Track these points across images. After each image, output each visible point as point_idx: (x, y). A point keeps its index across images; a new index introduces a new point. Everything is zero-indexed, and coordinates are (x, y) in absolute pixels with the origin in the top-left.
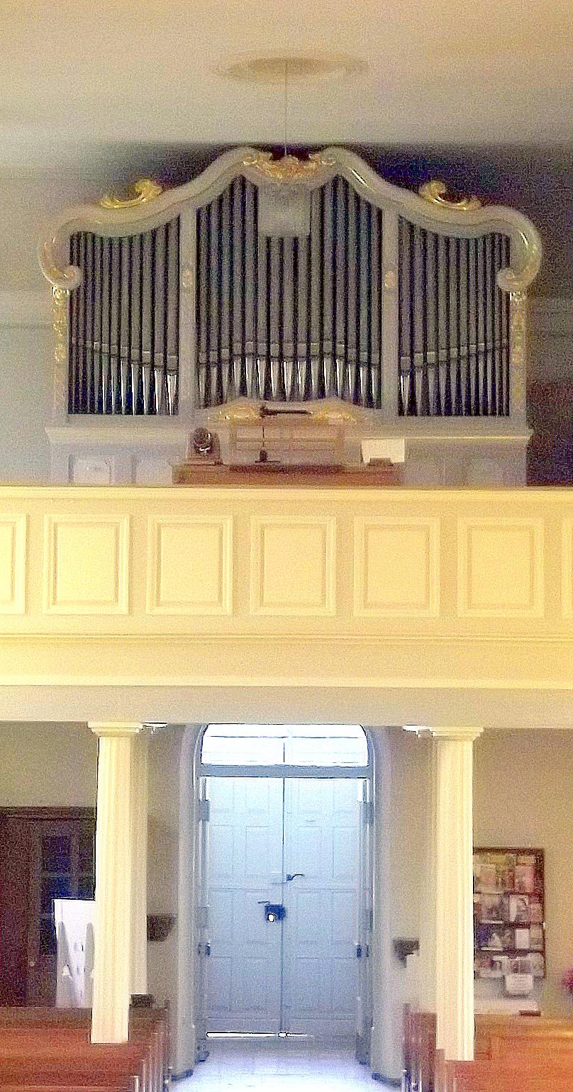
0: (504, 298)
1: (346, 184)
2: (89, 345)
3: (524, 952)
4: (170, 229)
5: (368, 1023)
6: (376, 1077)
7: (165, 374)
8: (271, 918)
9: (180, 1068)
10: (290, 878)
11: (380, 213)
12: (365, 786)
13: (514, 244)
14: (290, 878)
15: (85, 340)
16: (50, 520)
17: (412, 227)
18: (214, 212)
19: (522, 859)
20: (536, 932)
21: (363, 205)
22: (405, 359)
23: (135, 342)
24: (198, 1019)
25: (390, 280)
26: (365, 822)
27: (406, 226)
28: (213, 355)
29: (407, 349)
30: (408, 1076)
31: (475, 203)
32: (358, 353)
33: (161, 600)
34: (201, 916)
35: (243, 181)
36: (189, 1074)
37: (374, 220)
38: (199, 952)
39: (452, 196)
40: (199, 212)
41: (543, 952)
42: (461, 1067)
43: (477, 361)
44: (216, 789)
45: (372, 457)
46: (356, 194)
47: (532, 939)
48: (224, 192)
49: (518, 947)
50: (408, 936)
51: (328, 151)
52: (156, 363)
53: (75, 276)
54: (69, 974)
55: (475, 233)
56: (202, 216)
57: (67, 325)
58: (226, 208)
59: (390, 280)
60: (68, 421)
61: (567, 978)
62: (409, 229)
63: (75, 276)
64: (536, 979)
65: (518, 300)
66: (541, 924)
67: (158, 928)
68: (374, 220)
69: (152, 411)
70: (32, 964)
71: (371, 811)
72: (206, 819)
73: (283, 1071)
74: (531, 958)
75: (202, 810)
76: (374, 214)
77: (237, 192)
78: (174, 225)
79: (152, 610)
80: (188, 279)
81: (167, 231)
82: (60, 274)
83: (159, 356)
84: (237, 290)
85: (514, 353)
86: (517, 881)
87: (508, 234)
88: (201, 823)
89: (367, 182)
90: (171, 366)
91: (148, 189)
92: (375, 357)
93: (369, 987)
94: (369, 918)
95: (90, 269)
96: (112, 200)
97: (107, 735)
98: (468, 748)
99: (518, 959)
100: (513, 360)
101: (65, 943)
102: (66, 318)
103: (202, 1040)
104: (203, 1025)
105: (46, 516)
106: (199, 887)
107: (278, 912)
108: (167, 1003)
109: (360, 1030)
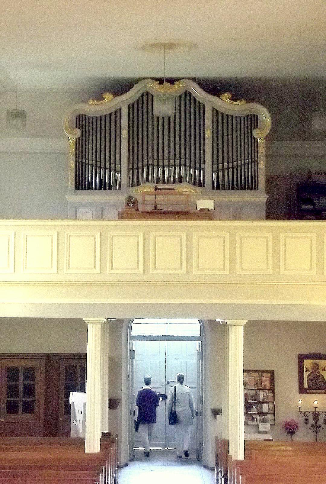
1: (190, 94)
2: (84, 161)
3: (266, 414)
6: (205, 467)
10: (168, 383)
11: (204, 106)
14: (168, 383)
17: (217, 111)
19: (265, 375)
20: (271, 405)
21: (197, 103)
30: (217, 466)
31: (243, 102)
35: (147, 93)
36: (126, 465)
39: (234, 98)
41: (274, 414)
42: (239, 462)
44: (137, 345)
46: (194, 98)
50: (217, 407)
51: (183, 80)
55: (245, 114)
56: (131, 107)
62: (216, 112)
63: (78, 133)
70: (61, 419)
71: (202, 355)
74: (269, 417)
75: (132, 354)
90: (118, 169)
91: (108, 96)
98: (241, 329)
99: (264, 417)
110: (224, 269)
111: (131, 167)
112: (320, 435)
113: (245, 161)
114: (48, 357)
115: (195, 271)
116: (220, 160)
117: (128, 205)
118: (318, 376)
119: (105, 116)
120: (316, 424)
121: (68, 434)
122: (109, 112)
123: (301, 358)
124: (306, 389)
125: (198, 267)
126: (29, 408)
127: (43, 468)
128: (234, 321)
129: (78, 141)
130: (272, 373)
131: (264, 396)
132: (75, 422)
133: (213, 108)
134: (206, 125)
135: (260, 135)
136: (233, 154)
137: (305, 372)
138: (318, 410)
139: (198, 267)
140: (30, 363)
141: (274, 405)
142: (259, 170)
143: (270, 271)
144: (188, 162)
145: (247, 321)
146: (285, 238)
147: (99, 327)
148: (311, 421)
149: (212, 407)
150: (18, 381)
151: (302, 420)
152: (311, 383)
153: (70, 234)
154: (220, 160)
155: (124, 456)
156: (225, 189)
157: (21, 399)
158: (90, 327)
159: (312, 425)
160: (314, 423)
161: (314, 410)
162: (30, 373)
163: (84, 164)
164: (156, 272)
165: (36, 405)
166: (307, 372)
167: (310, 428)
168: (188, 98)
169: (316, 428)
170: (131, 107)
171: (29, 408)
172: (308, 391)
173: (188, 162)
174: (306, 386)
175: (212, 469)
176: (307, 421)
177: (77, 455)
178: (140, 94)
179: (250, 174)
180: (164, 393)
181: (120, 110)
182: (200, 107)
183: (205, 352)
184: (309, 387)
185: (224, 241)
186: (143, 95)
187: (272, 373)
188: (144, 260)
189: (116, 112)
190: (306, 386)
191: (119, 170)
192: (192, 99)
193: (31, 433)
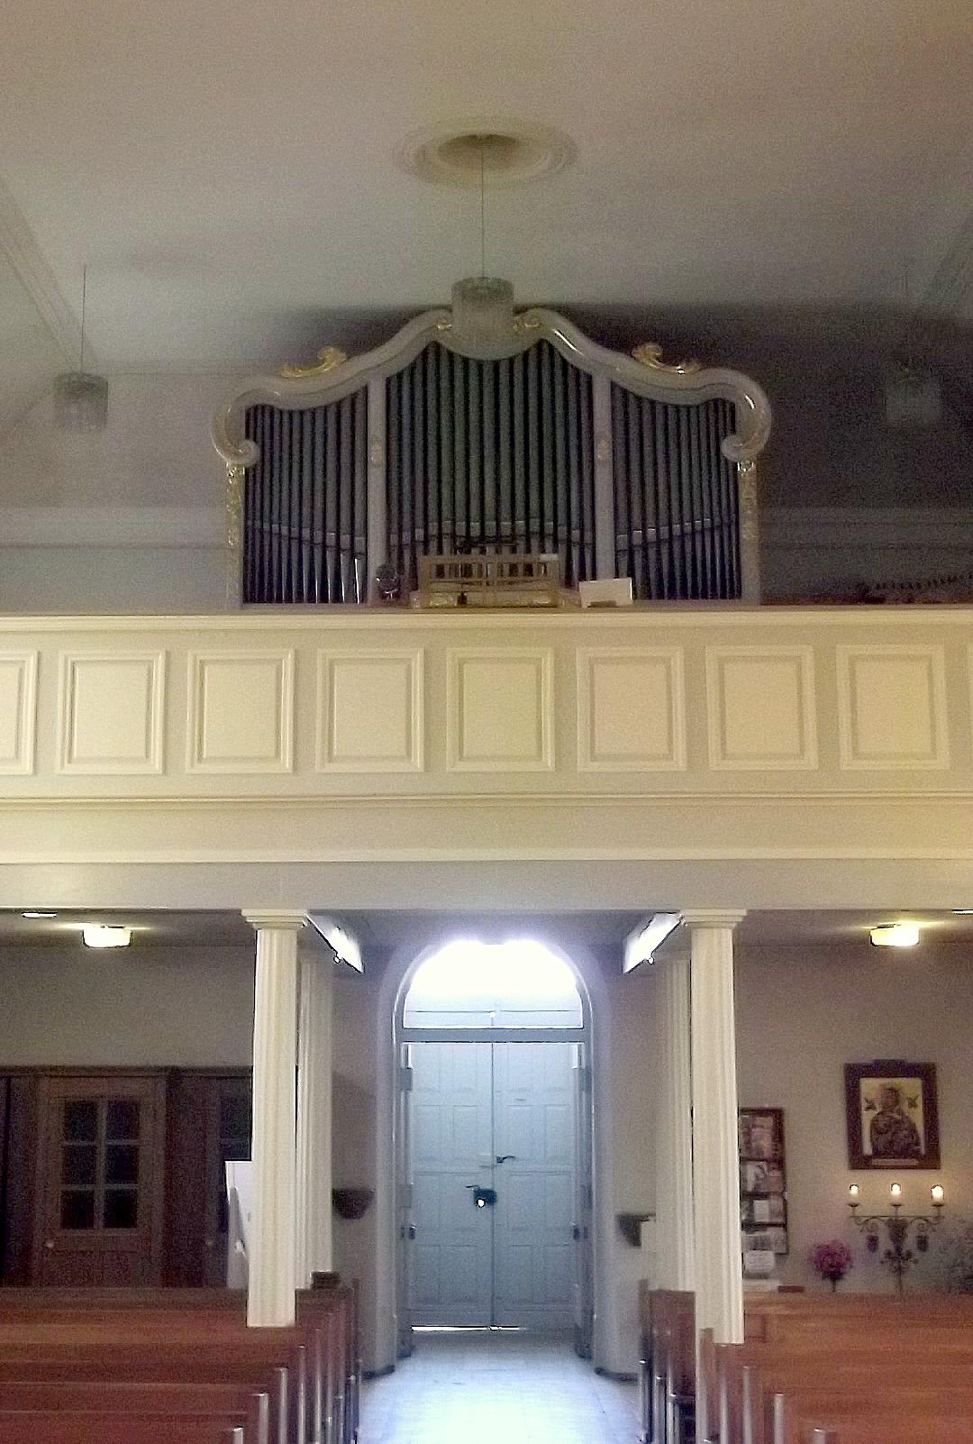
0: (731, 467)
1: (551, 348)
2: (266, 527)
3: (763, 1226)
4: (358, 400)
5: (589, 1313)
6: (600, 1372)
7: (353, 557)
8: (481, 1203)
9: (380, 1365)
10: (500, 1160)
11: (590, 378)
12: (580, 1052)
13: (739, 406)
14: (500, 1160)
15: (262, 521)
16: (195, 656)
17: (625, 393)
18: (406, 380)
19: (759, 1120)
20: (776, 1203)
21: (570, 371)
22: (623, 537)
23: (318, 524)
24: (402, 1310)
25: (603, 451)
26: (581, 1089)
27: (618, 395)
29: (622, 521)
30: (649, 1369)
31: (695, 366)
32: (569, 532)
33: (335, 753)
34: (404, 1196)
35: (437, 346)
36: (390, 1370)
37: (583, 388)
38: (403, 1236)
39: (669, 358)
40: (388, 381)
41: (784, 1226)
42: (721, 1354)
43: (703, 537)
44: (416, 1054)
46: (562, 357)
47: (772, 1212)
48: (416, 359)
49: (758, 1220)
50: (634, 1208)
51: (531, 312)
52: (342, 546)
53: (250, 451)
54: (242, 1250)
55: (694, 399)
56: (393, 384)
57: (242, 506)
58: (418, 378)
59: (603, 451)
60: (242, 606)
61: (814, 1254)
62: (621, 395)
63: (250, 451)
64: (779, 1255)
65: (746, 470)
66: (781, 1194)
67: (348, 1203)
68: (583, 388)
69: (337, 599)
70: (210, 1243)
71: (587, 1077)
72: (409, 1088)
73: (494, 1366)
74: (771, 1233)
75: (404, 1078)
76: (583, 380)
77: (431, 356)
78: (361, 396)
79: (323, 765)
80: (377, 453)
81: (353, 405)
82: (232, 448)
83: (345, 539)
84: (432, 485)
85: (745, 528)
86: (753, 1144)
87: (733, 400)
88: (403, 1094)
89: (573, 344)
90: (359, 547)
91: (332, 359)
92: (588, 538)
93: (588, 1274)
94: (587, 1197)
95: (267, 441)
96: (294, 370)
97: (266, 925)
98: (726, 939)
99: (757, 1234)
100: (744, 536)
101: (238, 1212)
102: (240, 499)
103: (406, 1332)
104: (408, 1318)
105: (190, 653)
106: (400, 1148)
107: (489, 1197)
108: (356, 1283)
109: (579, 1321)
110: (669, 756)
111: (394, 539)
112: (908, 1280)
113: (703, 522)
114: (174, 1076)
115: (583, 764)
116: (637, 520)
117: (384, 597)
118: (897, 1122)
119: (326, 408)
120: (898, 1249)
121: (224, 1282)
122: (332, 398)
123: (854, 1074)
124: (868, 1158)
125: (592, 752)
126: (122, 1212)
128: (699, 912)
129: (251, 474)
130: (778, 1114)
131: (757, 1177)
132: (239, 1245)
133: (613, 386)
134: (597, 429)
135: (742, 453)
136: (669, 508)
137: (864, 1112)
138: (901, 1212)
139: (592, 752)
140: (132, 1089)
141: (785, 1203)
142: (743, 548)
143: (812, 759)
144: (549, 525)
145: (744, 913)
146: (853, 661)
147: (291, 939)
148: (885, 1243)
149: (619, 1211)
150: (111, 1149)
151: (861, 1241)
152: (883, 1139)
153: (202, 658)
154: (637, 520)
155: (381, 1345)
156: (650, 597)
157: (101, 1189)
158: (262, 937)
159: (888, 1254)
160: (890, 1246)
161: (890, 1211)
162: (125, 1115)
163: (266, 536)
164: (462, 767)
165: (142, 1204)
166: (871, 1111)
167: (882, 1262)
168: (546, 357)
169: (898, 1259)
170: (394, 383)
171: (122, 1212)
172: (875, 1162)
173: (549, 525)
174: (867, 1149)
175: (625, 1379)
176: (873, 1243)
177: (223, 1334)
178: (416, 351)
179: (718, 551)
180: (489, 1187)
181: (366, 389)
182: (579, 382)
183: (597, 1063)
184: (877, 1153)
185: (668, 675)
186: (425, 354)
187: (778, 1114)
188: (427, 689)
189: (354, 397)
190: (867, 1149)
191: (363, 550)
192: (558, 361)
193: (125, 1277)
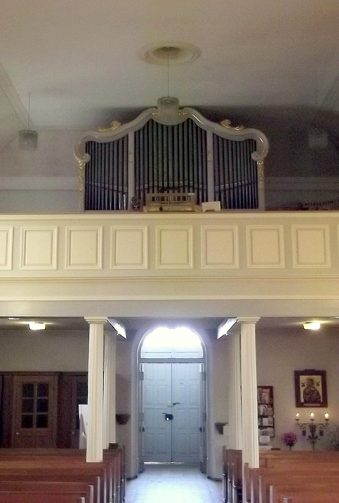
0: (255, 163)
1: (192, 121)
2: (93, 183)
3: (266, 427)
4: (125, 139)
5: (205, 457)
6: (209, 478)
7: (123, 194)
8: (168, 419)
9: (132, 475)
10: (174, 404)
11: (205, 132)
12: (202, 366)
13: (258, 141)
14: (174, 404)
15: (91, 181)
16: (68, 229)
17: (218, 137)
18: (141, 132)
19: (264, 390)
20: (270, 419)
21: (199, 129)
23: (111, 182)
24: (140, 456)
25: (210, 157)
26: (202, 380)
27: (215, 137)
28: (142, 187)
29: (217, 182)
30: (226, 477)
31: (242, 127)
32: (198, 185)
34: (141, 416)
35: (152, 121)
36: (136, 477)
37: (203, 135)
38: (140, 430)
39: (233, 125)
40: (135, 133)
41: (273, 427)
42: (251, 472)
43: (245, 187)
44: (145, 367)
45: (207, 209)
46: (196, 124)
47: (269, 422)
48: (145, 125)
49: (264, 425)
50: (221, 421)
51: (185, 109)
52: (119, 190)
53: (87, 157)
54: (84, 435)
55: (242, 139)
56: (137, 134)
57: (84, 176)
58: (146, 132)
59: (210, 157)
60: (84, 211)
61: (284, 437)
62: (216, 138)
63: (87, 157)
64: (271, 437)
65: (260, 164)
66: (272, 416)
67: (121, 419)
68: (203, 135)
69: (117, 209)
70: (73, 433)
71: (205, 375)
72: (142, 379)
73: (172, 476)
74: (269, 430)
75: (141, 376)
76: (203, 132)
77: (150, 124)
78: (126, 138)
79: (112, 267)
80: (131, 158)
81: (123, 141)
82: (81, 156)
83: (120, 188)
84: (151, 169)
85: (259, 184)
86: (263, 399)
87: (255, 139)
88: (140, 381)
89: (200, 120)
90: (125, 191)
91: (116, 125)
92: (205, 187)
93: (205, 444)
94: (205, 417)
95: (93, 154)
96: (102, 129)
97: (93, 322)
98: (253, 327)
99: (264, 430)
100: (259, 187)
101: (83, 422)
102: (84, 174)
103: (141, 464)
104: (142, 459)
105: (66, 228)
106: (139, 400)
107: (170, 417)
108: (124, 447)
109: (202, 460)
110: (233, 263)
111: (137, 188)
112: (316, 446)
113: (245, 182)
114: (61, 375)
115: (203, 266)
116: (222, 181)
117: (134, 208)
118: (313, 391)
119: (113, 142)
120: (313, 435)
121: (78, 447)
122: (116, 139)
123: (298, 374)
124: (303, 403)
125: (206, 262)
126: (43, 422)
127: (26, 478)
128: (244, 318)
129: (87, 165)
130: (271, 388)
131: (264, 410)
132: (83, 434)
133: (214, 134)
134: (208, 150)
135: (258, 158)
136: (233, 177)
137: (301, 387)
138: (314, 422)
139: (206, 262)
140: (46, 379)
141: (274, 419)
142: (259, 191)
143: (283, 264)
144: (191, 183)
145: (259, 318)
146: (297, 230)
148: (308, 433)
149: (216, 422)
150: (39, 400)
151: (300, 432)
152: (307, 397)
153: (70, 229)
154: (222, 181)
155: (133, 468)
156: (226, 208)
157: (35, 414)
158: (91, 326)
159: (310, 437)
160: (310, 434)
161: (310, 422)
162: (44, 388)
163: (93, 187)
164: (161, 267)
165: (50, 419)
166: (303, 387)
167: (307, 440)
168: (190, 124)
169: (313, 439)
170: (137, 133)
171: (43, 422)
172: (305, 405)
173: (191, 183)
174: (302, 400)
175: (218, 480)
176: (304, 433)
177: (78, 465)
178: (145, 122)
179: (250, 192)
180: (170, 413)
181: (127, 136)
182: (202, 133)
184: (305, 402)
185: (233, 235)
186: (148, 123)
187: (271, 388)
188: (149, 240)
189: (123, 138)
190: (302, 400)
191: (127, 192)
192: (194, 126)
193: (43, 445)
